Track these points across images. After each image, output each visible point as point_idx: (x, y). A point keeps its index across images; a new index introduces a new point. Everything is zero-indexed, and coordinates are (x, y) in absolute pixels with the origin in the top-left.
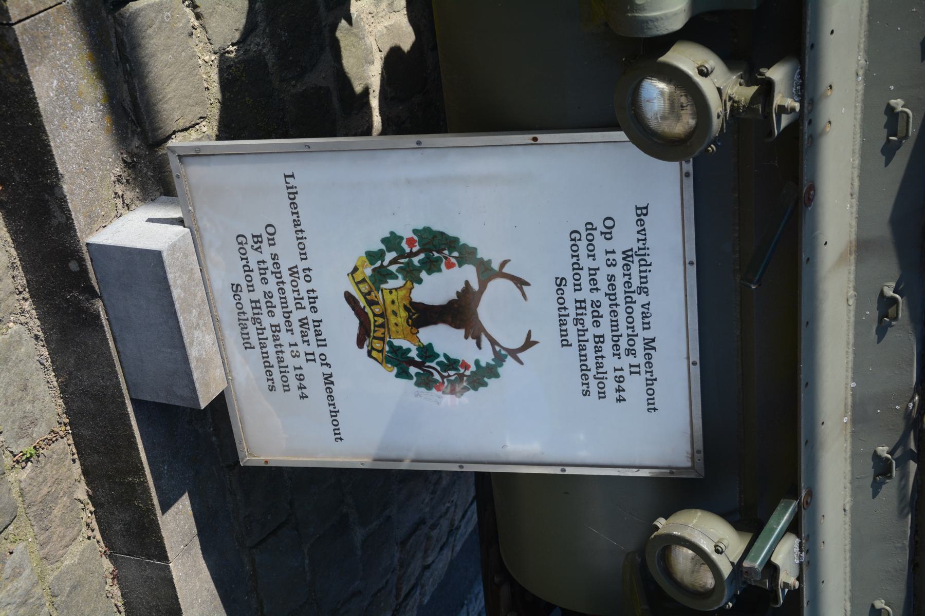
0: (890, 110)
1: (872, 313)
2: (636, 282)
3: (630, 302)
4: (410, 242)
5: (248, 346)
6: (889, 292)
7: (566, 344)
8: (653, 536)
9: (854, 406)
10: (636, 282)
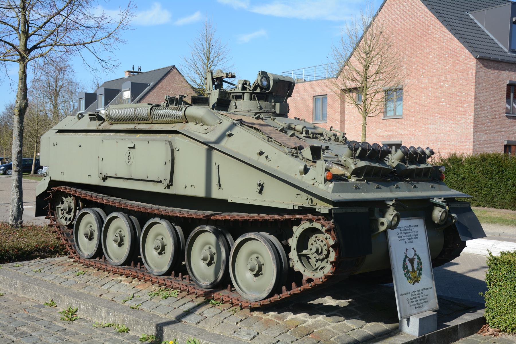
0: (376, 188)
1: (398, 189)
2: (403, 229)
3: (406, 230)
4: (405, 271)
5: (422, 306)
6: (395, 187)
7: (412, 242)
8: (309, 303)
9: (409, 192)
10: (403, 229)
